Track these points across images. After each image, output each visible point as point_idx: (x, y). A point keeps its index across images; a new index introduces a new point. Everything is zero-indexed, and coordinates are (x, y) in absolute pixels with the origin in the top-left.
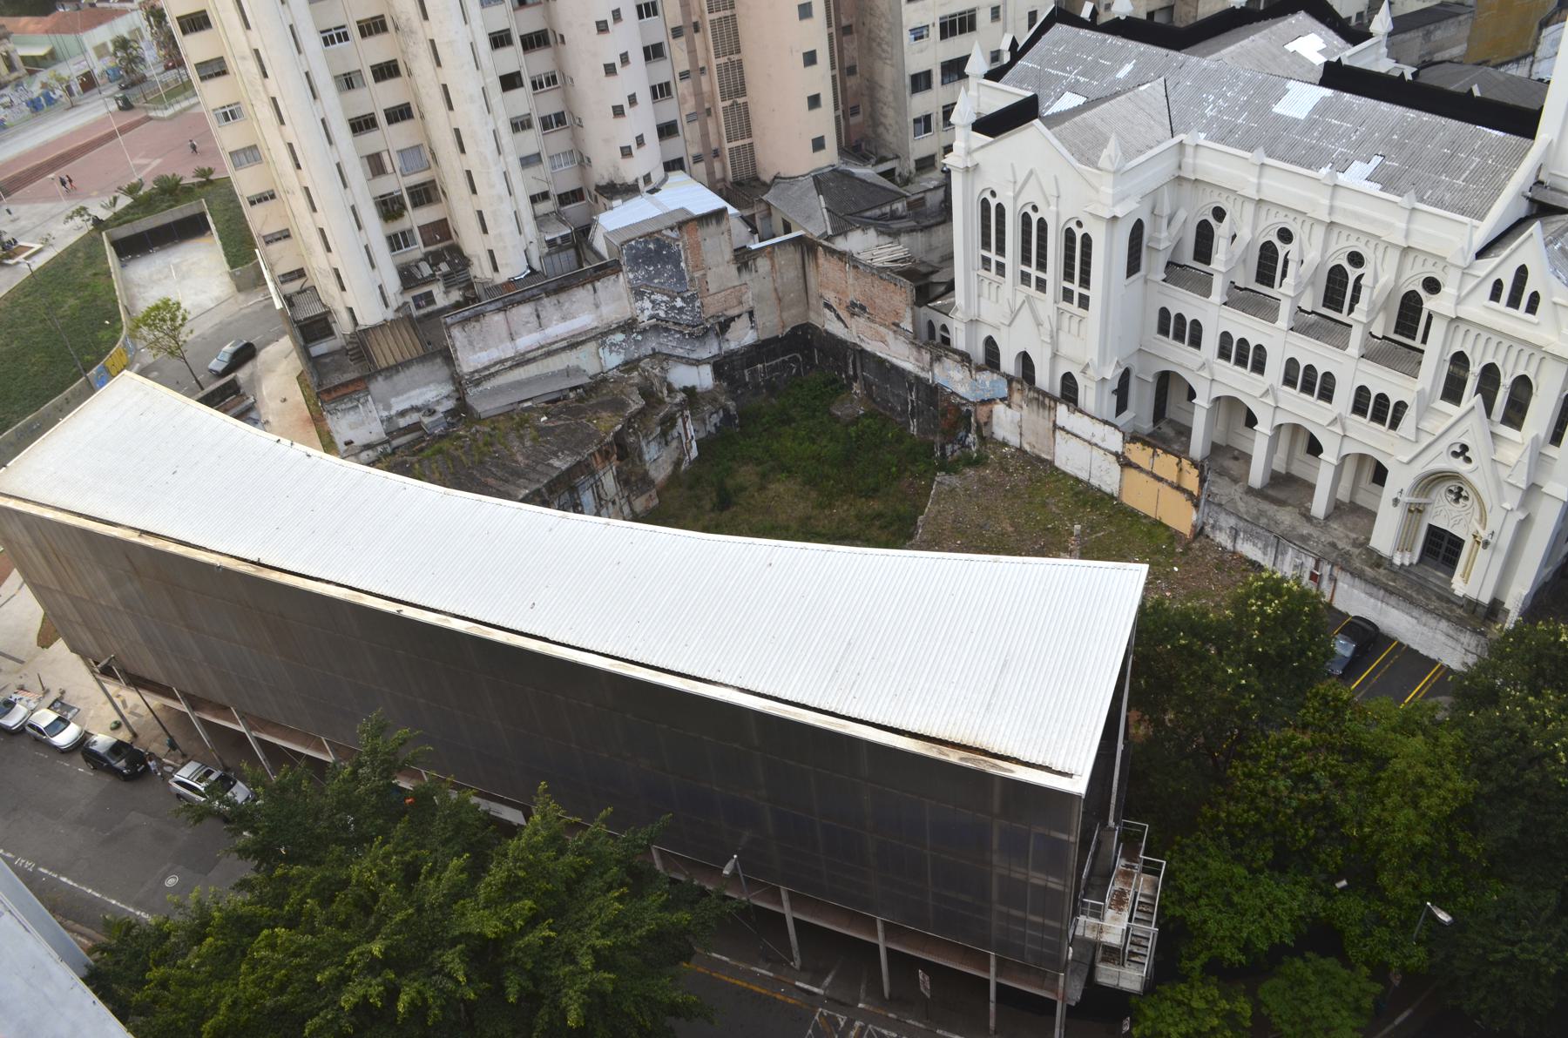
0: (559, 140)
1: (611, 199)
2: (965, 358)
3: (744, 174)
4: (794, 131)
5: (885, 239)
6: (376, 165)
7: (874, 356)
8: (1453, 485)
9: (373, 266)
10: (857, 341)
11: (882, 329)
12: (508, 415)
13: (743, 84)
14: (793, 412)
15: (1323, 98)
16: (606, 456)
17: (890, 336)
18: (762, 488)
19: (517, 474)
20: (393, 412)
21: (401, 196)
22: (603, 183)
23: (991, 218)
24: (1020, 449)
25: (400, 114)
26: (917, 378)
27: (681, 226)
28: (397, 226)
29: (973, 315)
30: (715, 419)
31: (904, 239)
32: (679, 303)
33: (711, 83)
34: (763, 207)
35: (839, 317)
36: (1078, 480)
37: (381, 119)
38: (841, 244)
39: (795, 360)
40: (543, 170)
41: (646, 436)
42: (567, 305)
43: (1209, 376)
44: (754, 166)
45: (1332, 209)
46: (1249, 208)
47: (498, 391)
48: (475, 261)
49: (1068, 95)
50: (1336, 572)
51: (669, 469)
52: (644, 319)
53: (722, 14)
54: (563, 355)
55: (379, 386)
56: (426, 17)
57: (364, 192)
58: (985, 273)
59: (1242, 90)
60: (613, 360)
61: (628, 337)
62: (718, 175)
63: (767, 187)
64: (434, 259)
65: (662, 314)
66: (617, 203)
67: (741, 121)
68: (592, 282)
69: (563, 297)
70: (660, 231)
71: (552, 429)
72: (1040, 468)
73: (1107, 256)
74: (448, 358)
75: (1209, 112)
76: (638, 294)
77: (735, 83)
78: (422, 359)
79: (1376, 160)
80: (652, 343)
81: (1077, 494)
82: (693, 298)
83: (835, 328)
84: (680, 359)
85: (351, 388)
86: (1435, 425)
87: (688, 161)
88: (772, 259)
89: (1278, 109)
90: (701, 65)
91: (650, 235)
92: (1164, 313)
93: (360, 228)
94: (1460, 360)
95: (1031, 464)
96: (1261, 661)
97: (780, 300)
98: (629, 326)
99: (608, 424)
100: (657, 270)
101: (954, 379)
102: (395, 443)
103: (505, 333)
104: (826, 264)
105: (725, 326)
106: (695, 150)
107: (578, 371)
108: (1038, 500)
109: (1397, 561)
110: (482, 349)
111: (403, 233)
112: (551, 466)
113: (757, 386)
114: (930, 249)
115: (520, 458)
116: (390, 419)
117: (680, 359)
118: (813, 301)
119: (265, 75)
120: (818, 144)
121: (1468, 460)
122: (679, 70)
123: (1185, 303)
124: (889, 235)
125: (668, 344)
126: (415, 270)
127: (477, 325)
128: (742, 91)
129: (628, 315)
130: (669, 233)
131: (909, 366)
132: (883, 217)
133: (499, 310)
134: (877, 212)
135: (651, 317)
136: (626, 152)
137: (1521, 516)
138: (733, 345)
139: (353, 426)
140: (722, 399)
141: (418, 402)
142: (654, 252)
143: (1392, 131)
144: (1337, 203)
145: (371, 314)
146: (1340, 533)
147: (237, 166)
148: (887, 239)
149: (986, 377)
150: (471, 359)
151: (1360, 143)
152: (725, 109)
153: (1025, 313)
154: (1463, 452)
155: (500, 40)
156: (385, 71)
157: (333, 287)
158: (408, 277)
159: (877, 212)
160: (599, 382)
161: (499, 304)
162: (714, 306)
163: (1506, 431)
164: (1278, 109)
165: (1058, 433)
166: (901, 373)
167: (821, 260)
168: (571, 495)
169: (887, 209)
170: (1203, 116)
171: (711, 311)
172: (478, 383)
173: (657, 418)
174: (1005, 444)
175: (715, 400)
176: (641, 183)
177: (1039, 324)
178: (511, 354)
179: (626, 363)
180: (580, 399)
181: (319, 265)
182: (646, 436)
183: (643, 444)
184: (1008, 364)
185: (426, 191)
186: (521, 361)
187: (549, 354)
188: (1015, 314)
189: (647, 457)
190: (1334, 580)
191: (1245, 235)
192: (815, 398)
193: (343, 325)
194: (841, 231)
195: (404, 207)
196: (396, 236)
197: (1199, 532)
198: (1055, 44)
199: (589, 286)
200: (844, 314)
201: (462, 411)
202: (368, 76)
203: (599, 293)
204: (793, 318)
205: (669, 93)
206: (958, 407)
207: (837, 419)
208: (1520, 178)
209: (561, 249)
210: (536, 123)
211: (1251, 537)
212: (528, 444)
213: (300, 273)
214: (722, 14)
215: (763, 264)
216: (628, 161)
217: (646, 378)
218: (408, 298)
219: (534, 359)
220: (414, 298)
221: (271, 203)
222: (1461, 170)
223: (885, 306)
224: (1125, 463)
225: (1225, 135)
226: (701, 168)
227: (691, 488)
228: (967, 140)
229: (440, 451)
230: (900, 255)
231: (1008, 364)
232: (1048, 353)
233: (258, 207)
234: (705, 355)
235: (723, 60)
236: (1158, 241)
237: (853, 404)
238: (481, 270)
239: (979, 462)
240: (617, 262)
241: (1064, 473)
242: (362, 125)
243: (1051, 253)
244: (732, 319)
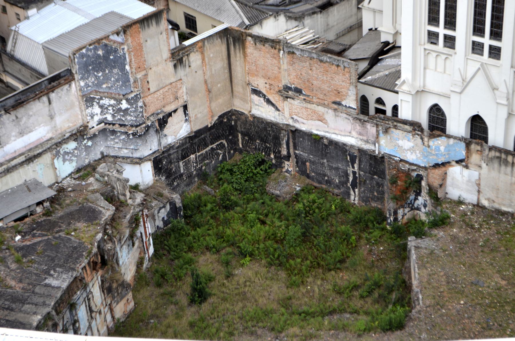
2: (415, 126)
7: (310, 135)
10: (291, 122)
17: (329, 115)
18: (229, 276)
19: (19, 300)
24: (478, 206)
26: (360, 150)
27: (126, 29)
29: (419, 85)
30: (163, 213)
31: (308, 21)
32: (124, 105)
35: (269, 102)
38: (256, 30)
39: (221, 146)
42: (24, 119)
52: (94, 125)
60: (66, 168)
61: (80, 144)
65: (110, 118)
66: (32, 12)
69: (21, 112)
70: (107, 37)
76: (89, 101)
80: (101, 147)
82: (137, 98)
88: (202, 53)
91: (98, 41)
95: (492, 218)
97: (209, 91)
98: (80, 134)
100: (104, 75)
101: (404, 148)
105: (163, 123)
113: (190, 176)
114: (328, 28)
115: (13, 283)
124: (296, 19)
125: (115, 146)
129: (79, 123)
130: (114, 38)
140: (166, 192)
148: (294, 23)
149: (439, 144)
162: (154, 104)
166: (341, 149)
168: (71, 311)
171: (152, 109)
174: (460, 202)
175: (161, 195)
177: (494, 89)
179: (78, 170)
180: (47, 213)
183: (118, 249)
184: (457, 125)
188: (466, 83)
194: (256, 21)
199: (45, 99)
204: (220, 107)
206: (407, 174)
212: (13, 266)
215: (195, 59)
217: (106, 184)
223: (325, 87)
227: (159, 285)
230: (309, 36)
231: (457, 125)
239: (440, 222)
240: (69, 71)
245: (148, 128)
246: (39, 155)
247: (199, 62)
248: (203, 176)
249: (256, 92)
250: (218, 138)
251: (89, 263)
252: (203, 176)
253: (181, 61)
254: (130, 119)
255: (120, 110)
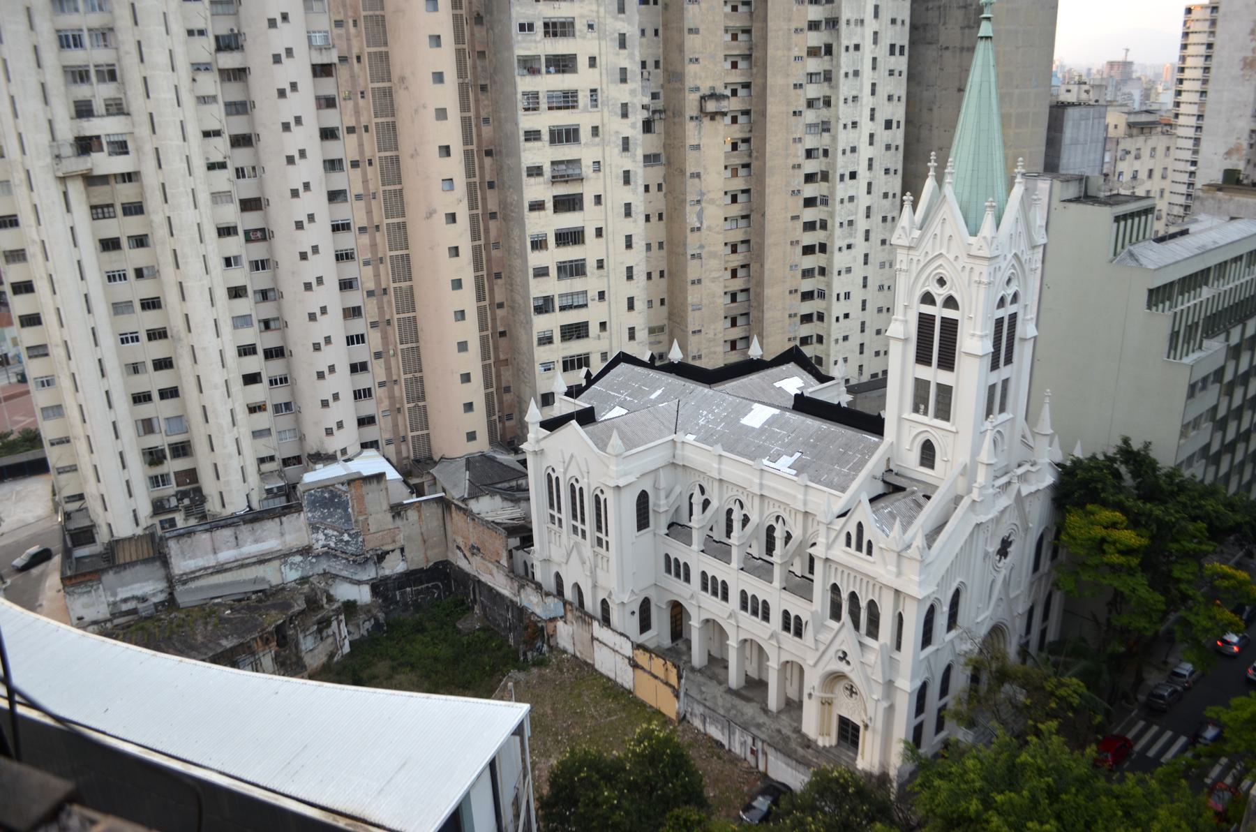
0: (285, 421)
1: (315, 463)
3: (423, 454)
4: (459, 427)
5: (508, 504)
6: (147, 426)
7: (485, 585)
8: (844, 683)
9: (131, 496)
11: (490, 565)
12: (201, 607)
13: (423, 392)
14: (427, 625)
15: (773, 416)
16: (266, 642)
17: (495, 571)
20: (118, 599)
21: (163, 450)
22: (313, 452)
23: (552, 484)
24: (574, 656)
25: (170, 393)
26: (511, 601)
28: (158, 470)
30: (368, 625)
32: (346, 537)
33: (400, 391)
34: (430, 478)
36: (609, 679)
37: (156, 396)
38: (474, 506)
39: (437, 587)
40: (272, 441)
41: (303, 631)
43: (702, 607)
44: (430, 450)
45: (761, 486)
46: (716, 484)
47: (201, 589)
48: (209, 498)
49: (617, 408)
50: (766, 747)
51: (324, 659)
53: (410, 345)
54: (253, 568)
55: (109, 578)
56: (190, 331)
57: (132, 445)
58: (551, 525)
59: (725, 409)
60: (292, 575)
62: (404, 454)
63: (436, 463)
64: (181, 496)
65: (332, 545)
67: (421, 418)
68: (279, 516)
69: (257, 525)
71: (230, 620)
72: (585, 669)
73: (622, 513)
74: (165, 561)
75: (701, 422)
76: (315, 528)
77: (418, 392)
78: (146, 561)
79: (797, 455)
80: (324, 565)
81: (605, 689)
82: (357, 535)
83: (462, 564)
84: (345, 579)
85: (88, 577)
86: (825, 637)
87: (382, 443)
89: (745, 421)
90: (395, 378)
91: (326, 487)
92: (667, 557)
93: (124, 467)
94: (835, 588)
96: (633, 787)
98: (306, 551)
99: (274, 619)
101: (531, 601)
102: (116, 621)
103: (209, 548)
104: (457, 517)
105: (381, 557)
106: (388, 436)
107: (263, 580)
108: (576, 691)
109: (820, 743)
110: (190, 558)
111: (162, 476)
112: (220, 645)
113: (406, 604)
116: (115, 604)
117: (345, 579)
118: (450, 544)
119: (70, 358)
120: (471, 436)
121: (848, 663)
122: (377, 381)
123: (679, 551)
125: (336, 567)
126: (165, 502)
127: (189, 540)
128: (422, 396)
129: (306, 543)
130: (340, 486)
131: (506, 592)
132: (511, 489)
133: (207, 530)
134: (506, 485)
135: (324, 546)
136: (329, 432)
137: (885, 704)
138: (388, 572)
139: (85, 606)
141: (139, 593)
142: (329, 498)
143: (811, 437)
144: (764, 482)
145: (125, 529)
146: (785, 724)
147: (45, 418)
148: (511, 504)
149: (551, 601)
150: (182, 564)
151: (790, 444)
152: (409, 409)
153: (575, 553)
154: (844, 657)
155: (247, 351)
156: (163, 364)
157: (100, 509)
158: (159, 507)
159: (506, 485)
160: (280, 589)
161: (207, 527)
162: (372, 543)
163: (869, 641)
164: (745, 421)
165: (595, 643)
167: (454, 515)
169: (514, 483)
170: (697, 424)
171: (369, 546)
172: (185, 583)
173: (315, 619)
174: (565, 652)
175: (369, 611)
176: (339, 454)
178: (212, 563)
180: (260, 601)
181: (91, 490)
182: (303, 631)
183: (301, 636)
185: (183, 448)
186: (220, 569)
187: (242, 566)
188: (569, 555)
189: (303, 648)
190: (765, 754)
191: (754, 518)
192: (448, 615)
193: (102, 537)
194: (474, 495)
195: (165, 457)
196: (156, 477)
197: (683, 719)
198: (618, 376)
200: (468, 554)
201: (170, 603)
202: (150, 366)
203: (285, 525)
204: (435, 556)
205: (370, 395)
206: (535, 623)
207: (459, 632)
208: (874, 464)
209: (276, 496)
210: (270, 408)
211: (715, 721)
213: (81, 497)
214: (410, 345)
215: (412, 515)
216: (330, 438)
217: (313, 590)
218: (156, 521)
219: (230, 569)
220: (161, 522)
221: (66, 446)
222: (848, 462)
224: (635, 665)
225: (707, 438)
226: (391, 450)
228: (537, 432)
229: (142, 628)
230: (518, 515)
231: (569, 593)
232: (590, 584)
233: (56, 448)
234: (365, 578)
235: (409, 376)
236: (659, 506)
237: (472, 622)
238: (213, 506)
239: (541, 663)
241: (602, 675)
242: (141, 398)
243: (585, 509)
244: (388, 553)
245: (367, 560)
246: (269, 560)
247: (416, 517)
248: (417, 607)
249: (459, 548)
250: (433, 580)
251: (261, 637)
252: (417, 607)
253: (399, 514)
254: (351, 549)
255: (342, 541)
